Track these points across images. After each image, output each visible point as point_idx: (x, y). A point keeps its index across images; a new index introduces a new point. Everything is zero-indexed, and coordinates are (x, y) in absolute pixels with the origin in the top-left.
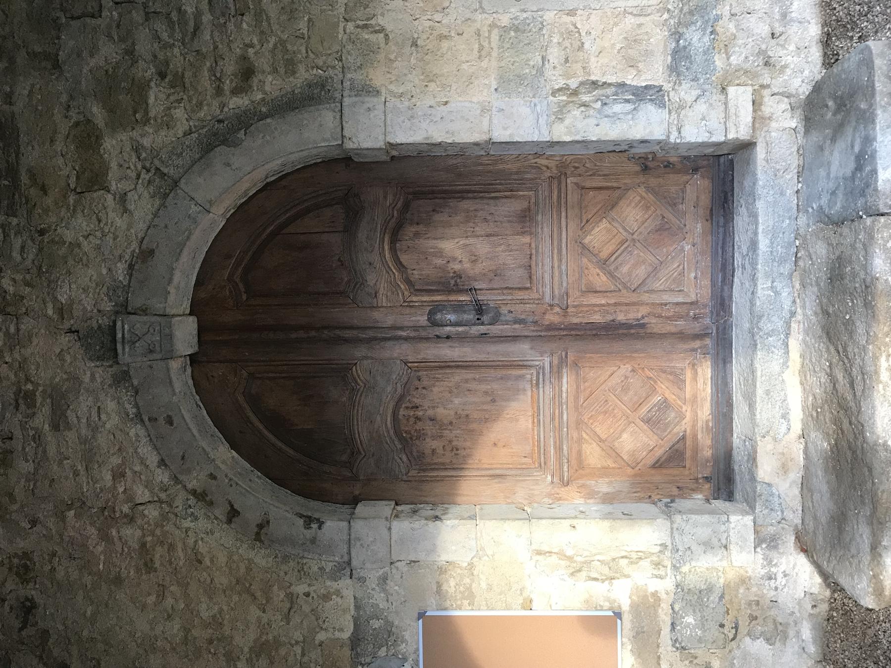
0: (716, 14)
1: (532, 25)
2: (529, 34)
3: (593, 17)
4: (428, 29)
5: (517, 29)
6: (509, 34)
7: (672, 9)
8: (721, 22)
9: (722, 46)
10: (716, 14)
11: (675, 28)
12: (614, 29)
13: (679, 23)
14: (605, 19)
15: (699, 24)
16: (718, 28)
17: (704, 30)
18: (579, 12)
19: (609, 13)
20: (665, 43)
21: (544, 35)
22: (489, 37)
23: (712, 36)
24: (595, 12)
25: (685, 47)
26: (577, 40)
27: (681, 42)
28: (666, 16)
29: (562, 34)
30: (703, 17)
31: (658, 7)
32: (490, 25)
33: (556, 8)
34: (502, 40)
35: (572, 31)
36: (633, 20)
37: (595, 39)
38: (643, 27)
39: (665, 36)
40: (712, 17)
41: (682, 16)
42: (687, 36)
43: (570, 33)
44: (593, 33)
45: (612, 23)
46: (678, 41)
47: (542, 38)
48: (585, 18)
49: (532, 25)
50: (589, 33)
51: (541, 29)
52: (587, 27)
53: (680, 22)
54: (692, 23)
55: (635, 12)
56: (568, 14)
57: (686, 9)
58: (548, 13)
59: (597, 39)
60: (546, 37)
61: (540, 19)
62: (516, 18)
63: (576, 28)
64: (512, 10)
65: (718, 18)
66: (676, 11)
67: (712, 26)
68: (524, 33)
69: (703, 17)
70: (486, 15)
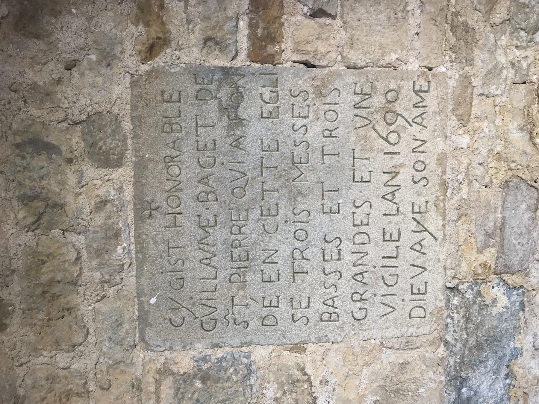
0: (515, 349)
1: (231, 370)
2: (227, 385)
3: (332, 354)
4: (43, 383)
5: (205, 378)
6: (192, 385)
7: (453, 342)
8: (520, 360)
9: (520, 393)
10: (515, 349)
11: (456, 371)
12: (364, 370)
13: (462, 362)
14: (351, 357)
15: (490, 363)
16: (515, 369)
17: (496, 372)
18: (310, 347)
19: (357, 350)
20: (440, 394)
21: (251, 386)
22: (157, 392)
23: (508, 381)
24: (335, 346)
25: (469, 399)
26: (306, 392)
27: (464, 390)
28: (442, 351)
29: (281, 385)
30: (495, 353)
31: (430, 337)
32: (159, 372)
33: (272, 341)
34: (180, 396)
35: (298, 381)
36: (392, 358)
37: (334, 390)
38: (409, 368)
39: (441, 382)
40: (508, 352)
41: (467, 352)
42: (473, 383)
43: (295, 383)
44: (333, 380)
45: (361, 362)
46: (460, 389)
47: (248, 392)
48: (319, 358)
49: (231, 370)
50: (325, 382)
51: (247, 377)
52: (323, 372)
53: (464, 363)
54: (481, 362)
55: (397, 346)
56: (291, 350)
57: (472, 341)
58: (259, 349)
59: (337, 388)
60: (254, 390)
61: (245, 361)
62: (205, 359)
63: (305, 374)
64: (199, 346)
65: (517, 353)
66: (458, 345)
67: (508, 366)
68: (217, 383)
69: (495, 353)
70: (151, 353)
